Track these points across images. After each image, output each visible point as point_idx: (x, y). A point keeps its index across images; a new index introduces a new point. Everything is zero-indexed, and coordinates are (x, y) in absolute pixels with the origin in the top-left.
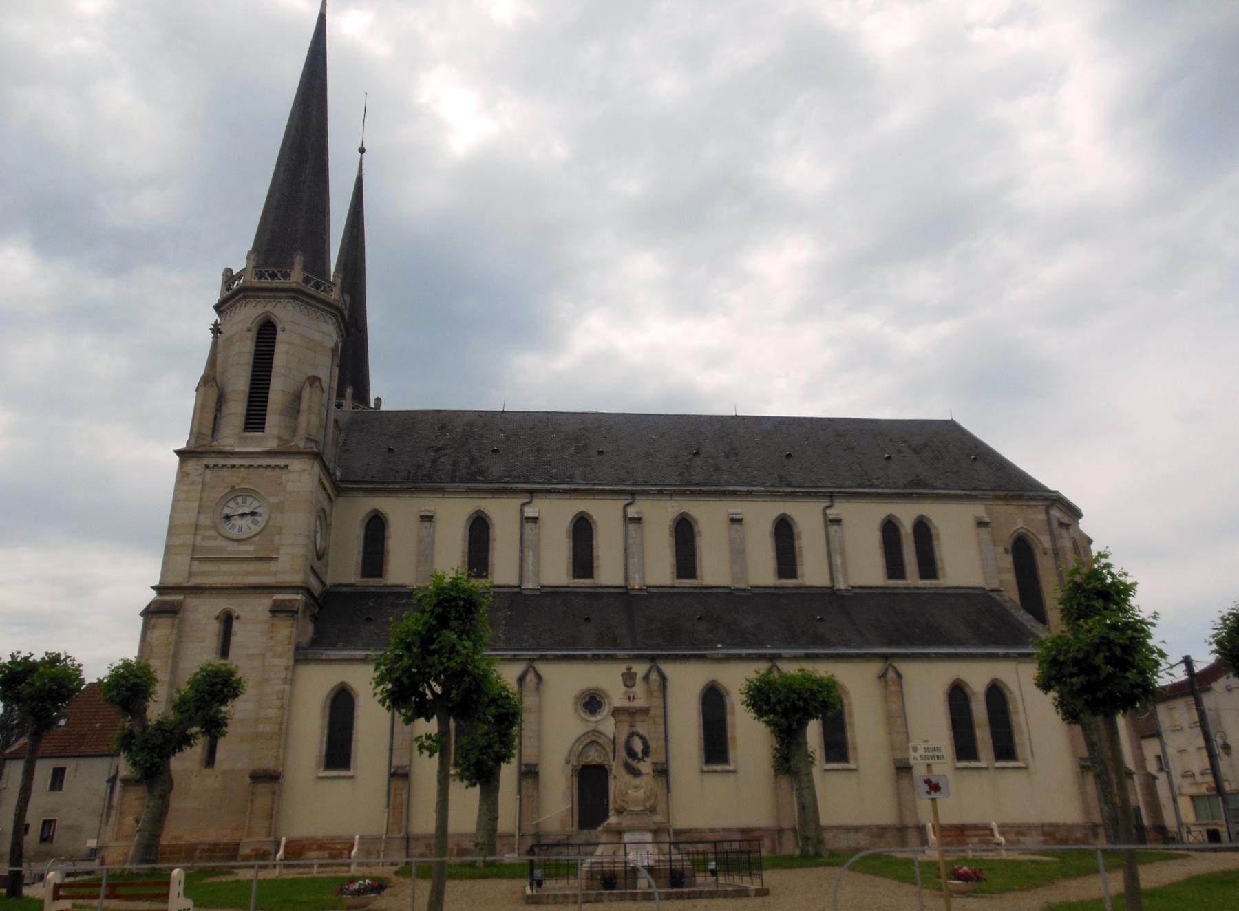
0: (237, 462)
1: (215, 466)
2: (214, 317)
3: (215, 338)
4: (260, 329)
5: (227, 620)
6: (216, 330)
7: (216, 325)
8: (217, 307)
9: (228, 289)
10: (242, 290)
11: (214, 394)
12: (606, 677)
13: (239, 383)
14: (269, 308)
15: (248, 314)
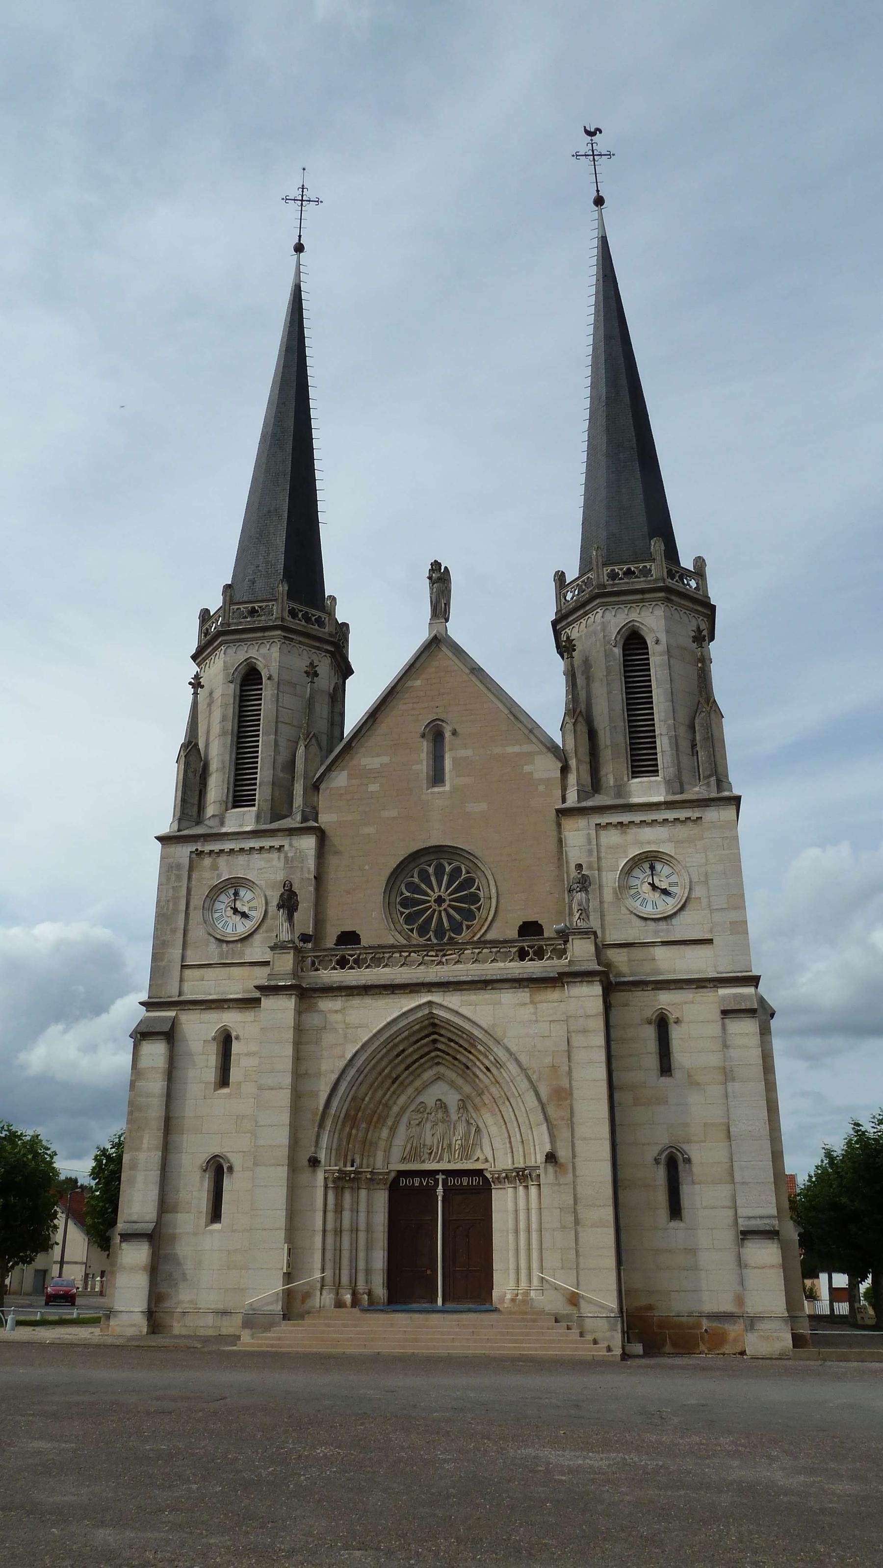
0: (228, 846)
1: (261, 848)
2: (193, 669)
3: (195, 694)
4: (625, 641)
5: (226, 1040)
6: (196, 684)
7: (197, 677)
8: (194, 658)
9: (206, 635)
10: (219, 634)
11: (583, 728)
12: (841, 1280)
13: (218, 753)
14: (634, 616)
15: (221, 665)
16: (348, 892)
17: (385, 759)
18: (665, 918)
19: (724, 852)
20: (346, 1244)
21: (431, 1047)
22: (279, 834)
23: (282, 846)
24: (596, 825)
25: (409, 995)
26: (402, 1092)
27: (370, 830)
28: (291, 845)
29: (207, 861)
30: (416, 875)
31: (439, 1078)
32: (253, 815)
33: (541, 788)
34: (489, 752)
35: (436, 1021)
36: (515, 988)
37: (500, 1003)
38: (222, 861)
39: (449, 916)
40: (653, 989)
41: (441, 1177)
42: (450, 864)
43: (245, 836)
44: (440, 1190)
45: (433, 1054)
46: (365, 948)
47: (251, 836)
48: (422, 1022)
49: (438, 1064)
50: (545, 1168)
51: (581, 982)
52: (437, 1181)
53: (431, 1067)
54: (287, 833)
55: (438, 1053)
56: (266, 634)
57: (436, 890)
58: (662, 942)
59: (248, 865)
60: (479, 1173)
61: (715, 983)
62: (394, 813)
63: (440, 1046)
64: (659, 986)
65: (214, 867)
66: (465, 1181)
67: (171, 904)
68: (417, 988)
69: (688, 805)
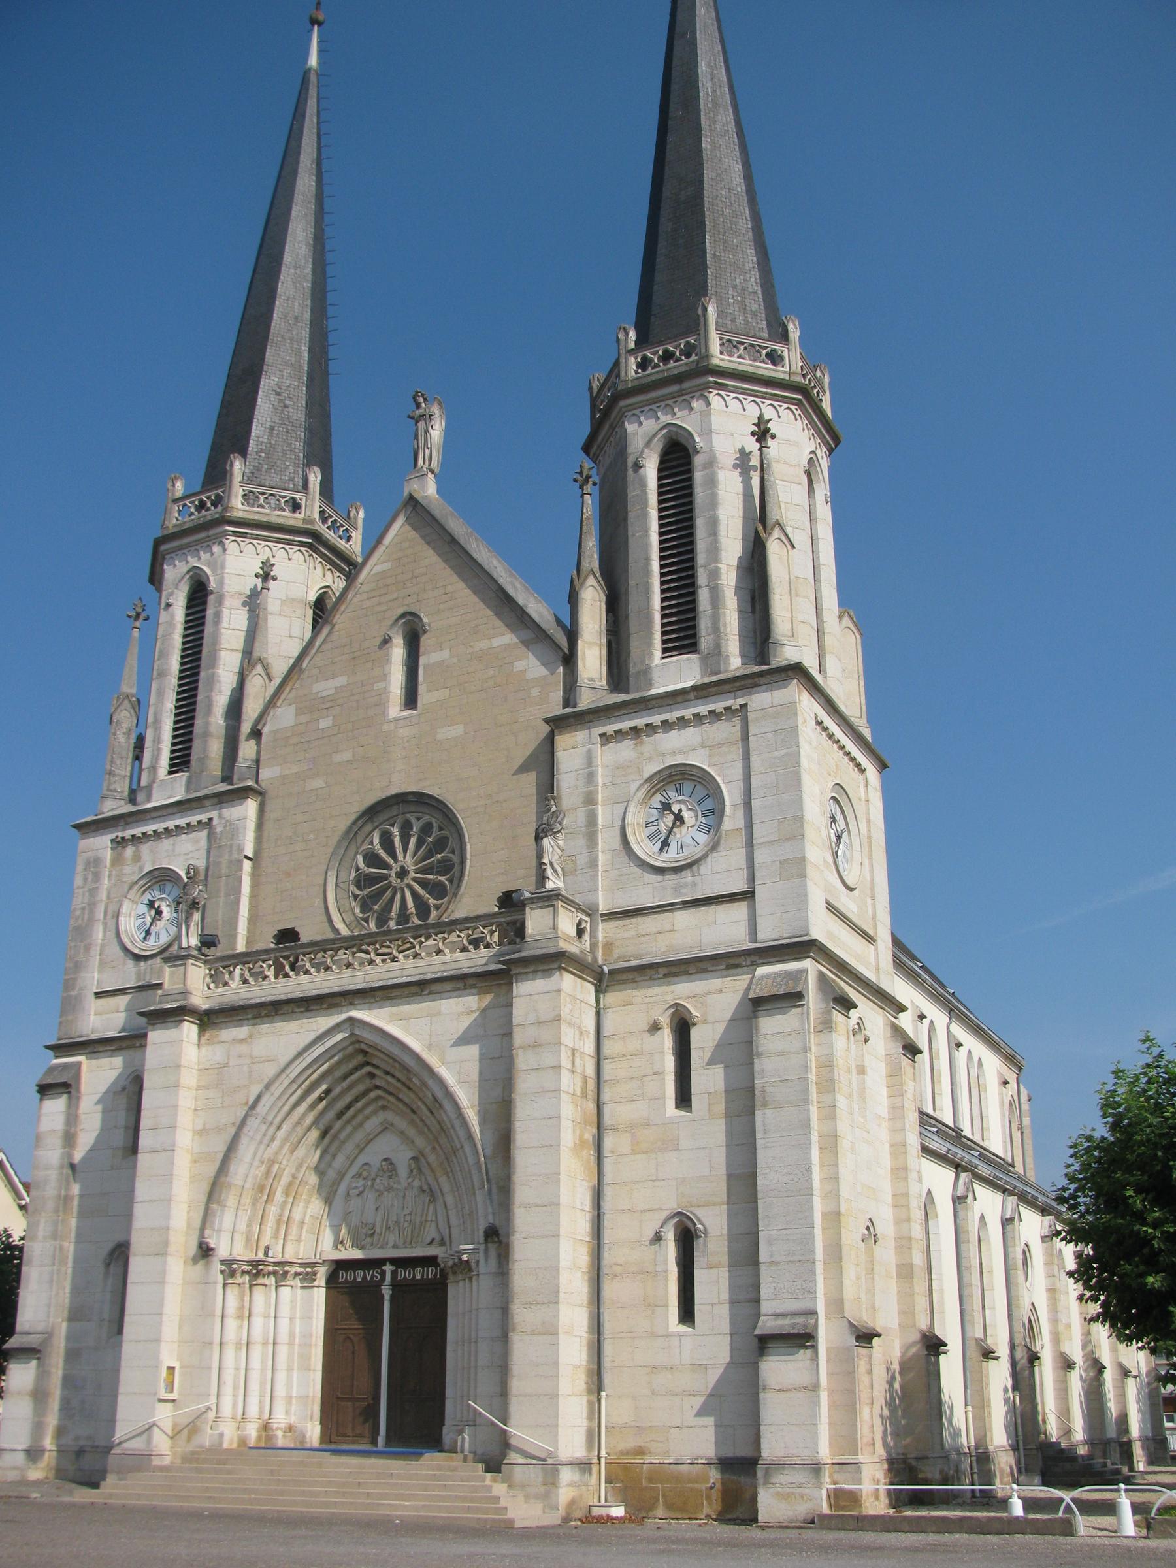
0: (149, 828)
16: (288, 875)
17: (341, 681)
18: (690, 866)
19: (776, 754)
20: (256, 1363)
21: (368, 1083)
22: (207, 802)
23: (210, 819)
24: (601, 735)
25: (329, 1011)
26: (339, 1149)
27: (318, 783)
28: (220, 816)
29: (129, 851)
30: (376, 841)
31: (386, 1127)
32: (184, 779)
33: (535, 692)
34: (470, 650)
35: (363, 1047)
36: (459, 989)
37: (439, 1013)
38: (145, 848)
39: (415, 895)
40: (665, 976)
41: (388, 1268)
42: (418, 819)
43: (170, 811)
44: (386, 1292)
45: (373, 1095)
46: (305, 945)
47: (175, 810)
48: (344, 1048)
49: (384, 1108)
50: (486, 1250)
51: (535, 972)
52: (383, 1273)
53: (375, 1112)
54: (215, 800)
55: (380, 1092)
56: (212, 532)
57: (401, 858)
58: (684, 903)
59: (173, 850)
60: (431, 1261)
61: (754, 958)
62: (347, 755)
63: (377, 1082)
64: (673, 970)
65: (137, 858)
66: (419, 1273)
67: (86, 912)
68: (336, 1000)
69: (727, 687)
